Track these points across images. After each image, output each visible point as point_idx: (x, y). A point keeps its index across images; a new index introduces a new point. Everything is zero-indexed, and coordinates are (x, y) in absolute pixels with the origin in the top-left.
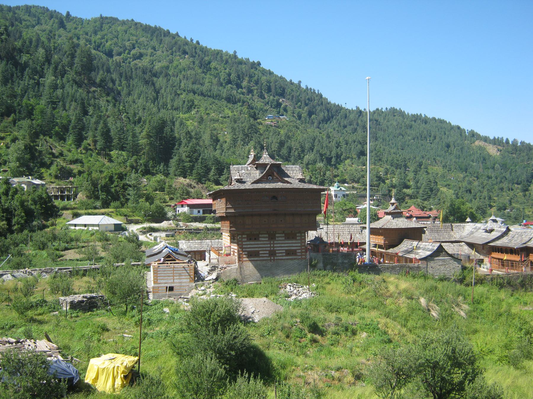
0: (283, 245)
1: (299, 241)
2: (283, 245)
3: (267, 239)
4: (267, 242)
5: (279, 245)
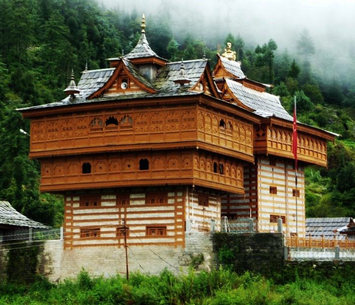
0: (142, 216)
1: (172, 208)
2: (142, 216)
3: (114, 204)
4: (114, 210)
5: (134, 216)
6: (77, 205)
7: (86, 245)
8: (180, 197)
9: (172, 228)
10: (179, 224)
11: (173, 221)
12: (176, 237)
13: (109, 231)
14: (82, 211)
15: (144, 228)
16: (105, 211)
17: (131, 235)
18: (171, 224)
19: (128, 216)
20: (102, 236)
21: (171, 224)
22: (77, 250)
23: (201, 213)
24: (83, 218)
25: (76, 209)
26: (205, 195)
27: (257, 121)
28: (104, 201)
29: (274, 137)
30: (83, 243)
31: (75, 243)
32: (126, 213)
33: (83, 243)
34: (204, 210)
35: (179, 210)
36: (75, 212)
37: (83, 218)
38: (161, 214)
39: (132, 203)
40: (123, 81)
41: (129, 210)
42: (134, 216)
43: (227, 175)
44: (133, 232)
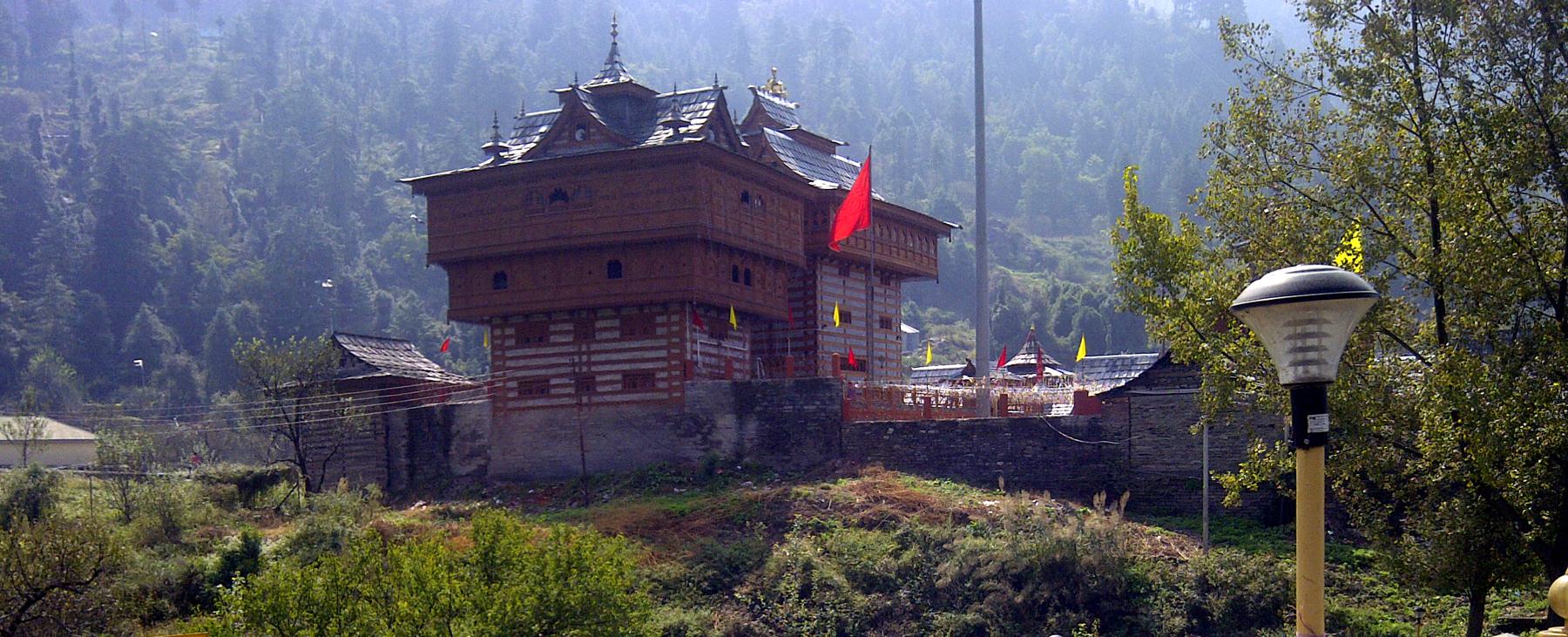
1: (664, 342)
2: (615, 357)
3: (570, 339)
4: (571, 349)
5: (603, 357)
6: (512, 342)
7: (529, 408)
8: (675, 324)
9: (511, 395)
10: (675, 368)
11: (665, 364)
12: (670, 390)
13: (563, 387)
14: (520, 352)
15: (619, 377)
16: (556, 350)
17: (599, 389)
18: (663, 370)
19: (594, 358)
20: (599, 389)
21: (663, 370)
22: (515, 416)
23: (713, 351)
24: (522, 363)
25: (510, 348)
26: (711, 316)
27: (813, 195)
28: (555, 333)
29: (925, 248)
30: (523, 404)
31: (511, 405)
32: (589, 353)
33: (523, 404)
34: (719, 346)
35: (675, 345)
36: (509, 354)
37: (522, 363)
38: (647, 354)
39: (553, 339)
40: (579, 127)
41: (594, 347)
42: (603, 357)
43: (758, 286)
44: (555, 386)
